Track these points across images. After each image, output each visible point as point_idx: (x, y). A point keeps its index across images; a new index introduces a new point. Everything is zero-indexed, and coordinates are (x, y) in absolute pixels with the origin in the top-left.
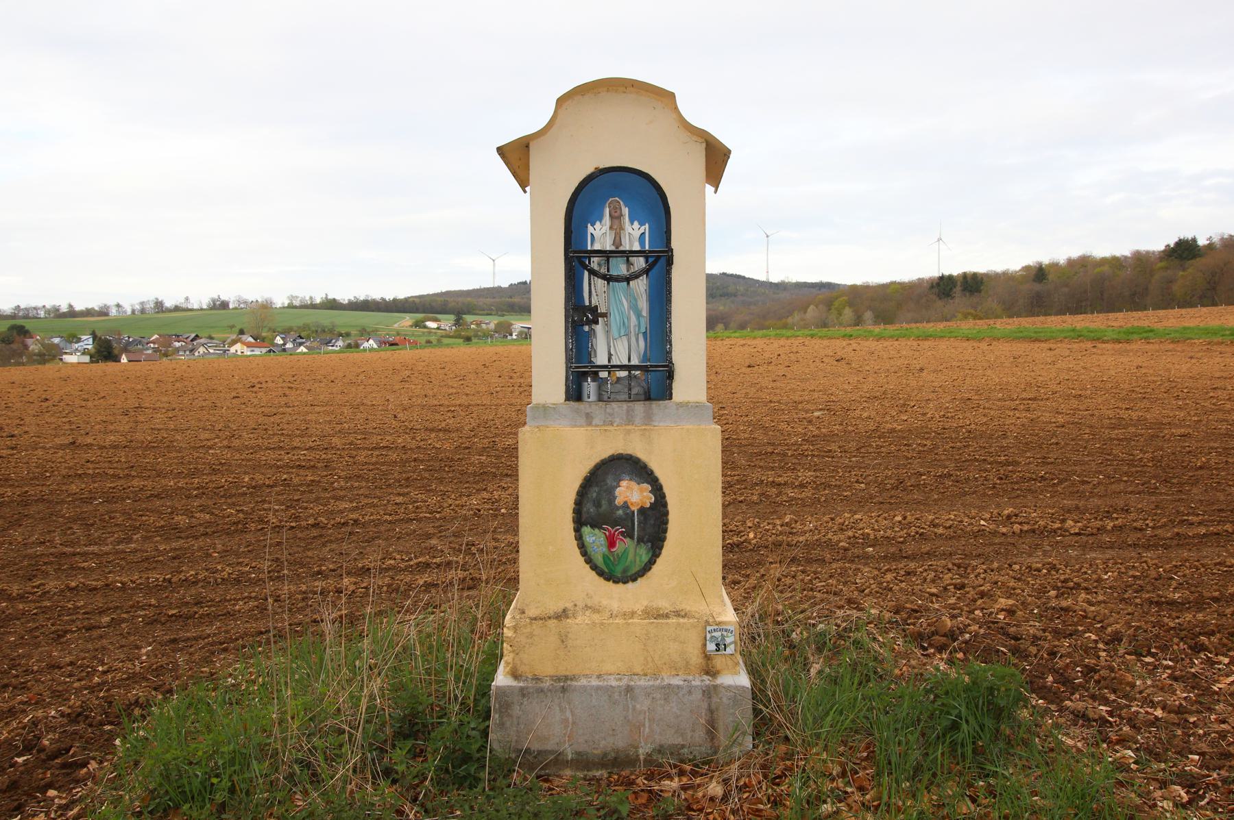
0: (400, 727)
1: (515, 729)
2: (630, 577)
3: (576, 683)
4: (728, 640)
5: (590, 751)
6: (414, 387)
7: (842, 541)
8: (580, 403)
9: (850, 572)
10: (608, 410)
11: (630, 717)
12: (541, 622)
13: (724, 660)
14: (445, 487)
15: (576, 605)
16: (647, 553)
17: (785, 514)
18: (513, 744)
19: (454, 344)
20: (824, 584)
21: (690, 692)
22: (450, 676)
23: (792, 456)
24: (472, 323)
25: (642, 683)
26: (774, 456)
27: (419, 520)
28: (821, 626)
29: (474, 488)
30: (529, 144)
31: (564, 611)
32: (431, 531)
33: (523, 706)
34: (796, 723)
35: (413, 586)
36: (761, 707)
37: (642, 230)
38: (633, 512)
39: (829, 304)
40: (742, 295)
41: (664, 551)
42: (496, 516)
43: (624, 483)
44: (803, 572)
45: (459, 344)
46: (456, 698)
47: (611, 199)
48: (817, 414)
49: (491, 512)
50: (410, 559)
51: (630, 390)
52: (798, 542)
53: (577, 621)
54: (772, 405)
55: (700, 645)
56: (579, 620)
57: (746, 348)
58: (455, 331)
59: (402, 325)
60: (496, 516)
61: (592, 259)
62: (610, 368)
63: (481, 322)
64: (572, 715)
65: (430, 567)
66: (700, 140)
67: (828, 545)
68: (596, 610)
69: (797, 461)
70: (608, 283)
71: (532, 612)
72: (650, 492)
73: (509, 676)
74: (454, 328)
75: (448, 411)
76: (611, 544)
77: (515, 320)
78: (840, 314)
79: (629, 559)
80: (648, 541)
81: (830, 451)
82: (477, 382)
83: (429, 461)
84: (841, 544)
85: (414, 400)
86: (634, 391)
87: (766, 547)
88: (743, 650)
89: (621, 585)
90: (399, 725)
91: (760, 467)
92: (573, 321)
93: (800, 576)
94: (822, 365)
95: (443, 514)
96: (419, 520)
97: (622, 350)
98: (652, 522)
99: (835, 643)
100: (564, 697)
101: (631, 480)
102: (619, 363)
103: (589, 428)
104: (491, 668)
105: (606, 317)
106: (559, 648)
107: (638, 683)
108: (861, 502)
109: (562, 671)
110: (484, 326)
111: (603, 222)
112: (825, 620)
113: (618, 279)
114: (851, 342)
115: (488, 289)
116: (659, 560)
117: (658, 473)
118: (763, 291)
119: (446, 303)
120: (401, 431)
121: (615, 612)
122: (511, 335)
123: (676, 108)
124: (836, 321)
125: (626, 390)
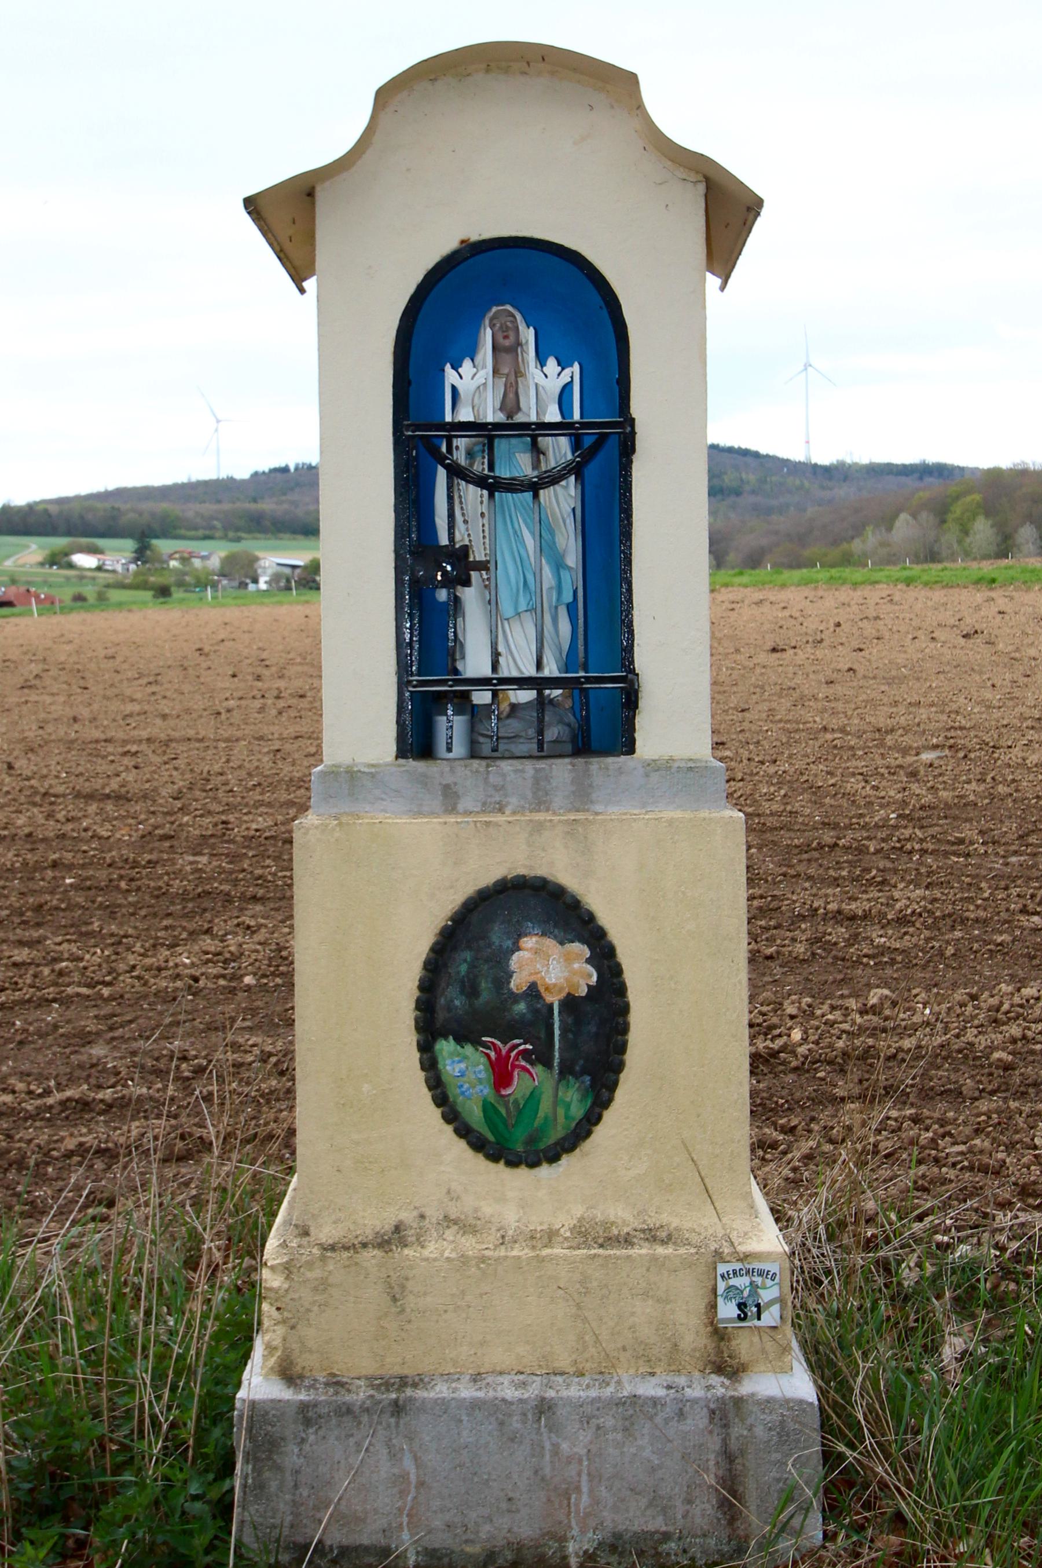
0: (31, 1491)
1: (288, 1497)
2: (545, 1151)
3: (425, 1394)
4: (766, 1295)
5: (457, 1549)
6: (48, 699)
7: (997, 1049)
8: (430, 762)
9: (1020, 1121)
10: (492, 779)
11: (547, 1471)
12: (346, 1254)
13: (756, 1339)
14: (121, 925)
15: (422, 1217)
16: (583, 1098)
17: (869, 986)
18: (286, 1532)
19: (134, 603)
20: (962, 1148)
21: (681, 1414)
22: (142, 1371)
23: (878, 852)
24: (171, 557)
25: (574, 1392)
26: (838, 852)
27: (65, 1001)
28: (963, 1249)
29: (184, 928)
30: (313, 188)
31: (397, 1229)
32: (92, 1027)
33: (307, 1447)
34: (921, 1484)
35: (55, 1153)
36: (842, 1448)
37: (565, 377)
38: (550, 1007)
39: (941, 510)
40: (753, 492)
41: (620, 1094)
42: (233, 991)
43: (529, 942)
44: (916, 1120)
45: (144, 603)
46: (155, 1422)
47: (494, 309)
48: (927, 756)
49: (222, 982)
50: (47, 1092)
51: (541, 732)
52: (900, 1049)
53: (426, 1253)
54: (829, 736)
55: (701, 1305)
56: (431, 1249)
57: (766, 608)
58: (137, 574)
59: (21, 562)
60: (233, 991)
61: (456, 442)
62: (496, 683)
63: (191, 555)
64: (417, 1467)
65: (92, 1110)
66: (693, 177)
67: (966, 1057)
68: (466, 1226)
69: (889, 865)
70: (491, 496)
71: (326, 1232)
72: (588, 961)
73: (275, 1378)
74: (133, 567)
75: (125, 754)
76: (501, 1075)
77: (266, 549)
78: (966, 532)
79: (541, 1114)
80: (584, 1072)
81: (961, 841)
82: (186, 688)
83: (83, 866)
84: (996, 1055)
85: (50, 728)
86: (552, 733)
87: (830, 1063)
88: (798, 1316)
89: (523, 1172)
90: (27, 1486)
91: (810, 878)
92: (415, 582)
93: (911, 1131)
94: (932, 645)
95: (117, 988)
96: (65, 1001)
97: (522, 642)
98: (593, 1028)
99: (996, 1287)
100: (397, 1424)
101: (544, 934)
102: (515, 674)
103: (452, 819)
104: (232, 1356)
105: (487, 569)
106: (386, 1314)
107: (564, 1393)
108: (1034, 957)
109: (393, 1367)
110: (197, 563)
111: (479, 358)
112: (972, 1236)
113: (513, 486)
114: (993, 594)
115: (206, 484)
116: (608, 1115)
117: (605, 918)
118: (798, 482)
119: (115, 514)
120: (23, 799)
121: (510, 1233)
122: (255, 581)
123: (640, 107)
124: (955, 546)
125: (532, 732)
